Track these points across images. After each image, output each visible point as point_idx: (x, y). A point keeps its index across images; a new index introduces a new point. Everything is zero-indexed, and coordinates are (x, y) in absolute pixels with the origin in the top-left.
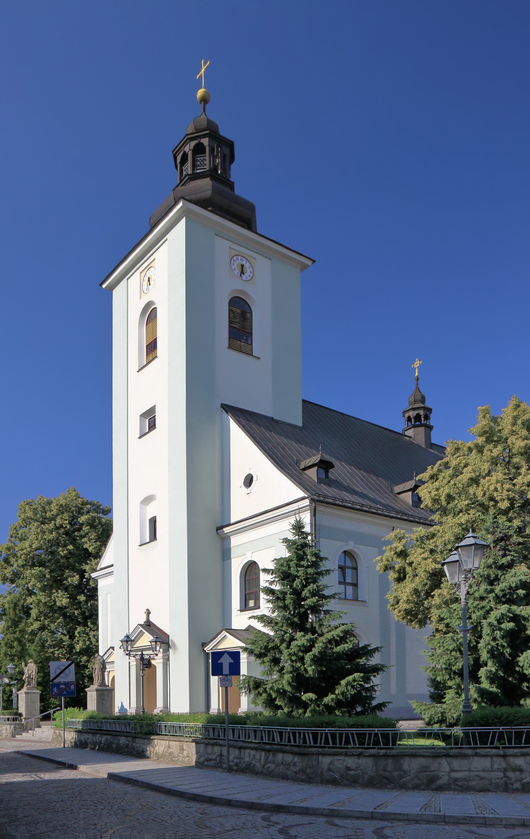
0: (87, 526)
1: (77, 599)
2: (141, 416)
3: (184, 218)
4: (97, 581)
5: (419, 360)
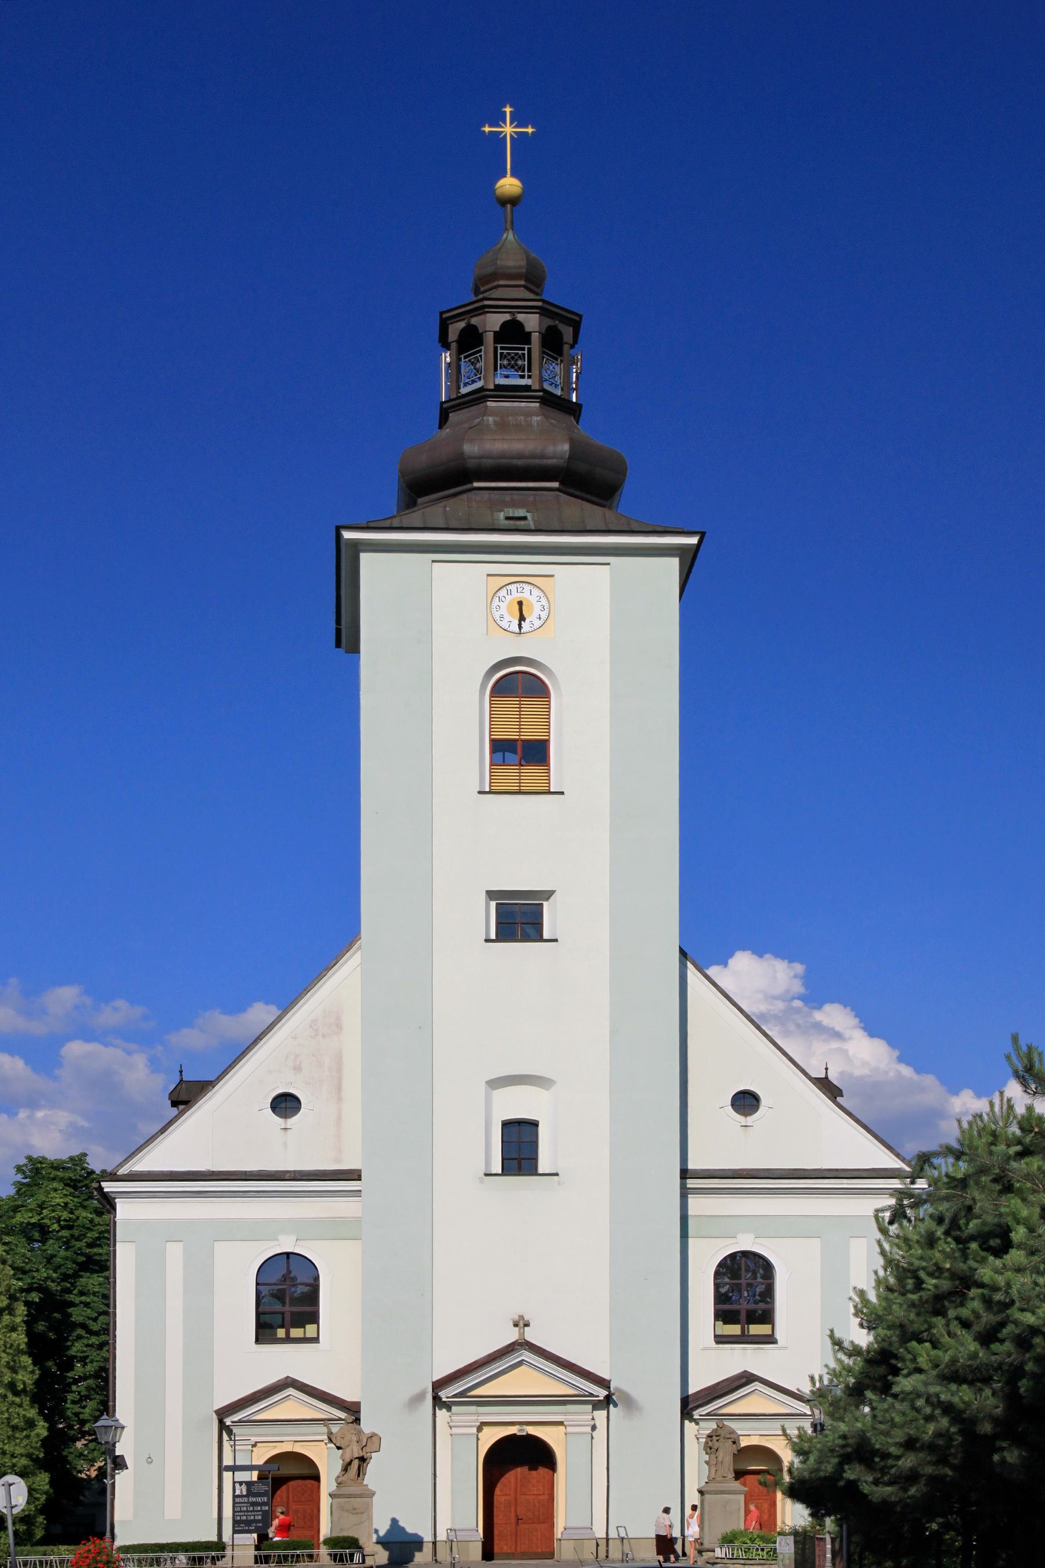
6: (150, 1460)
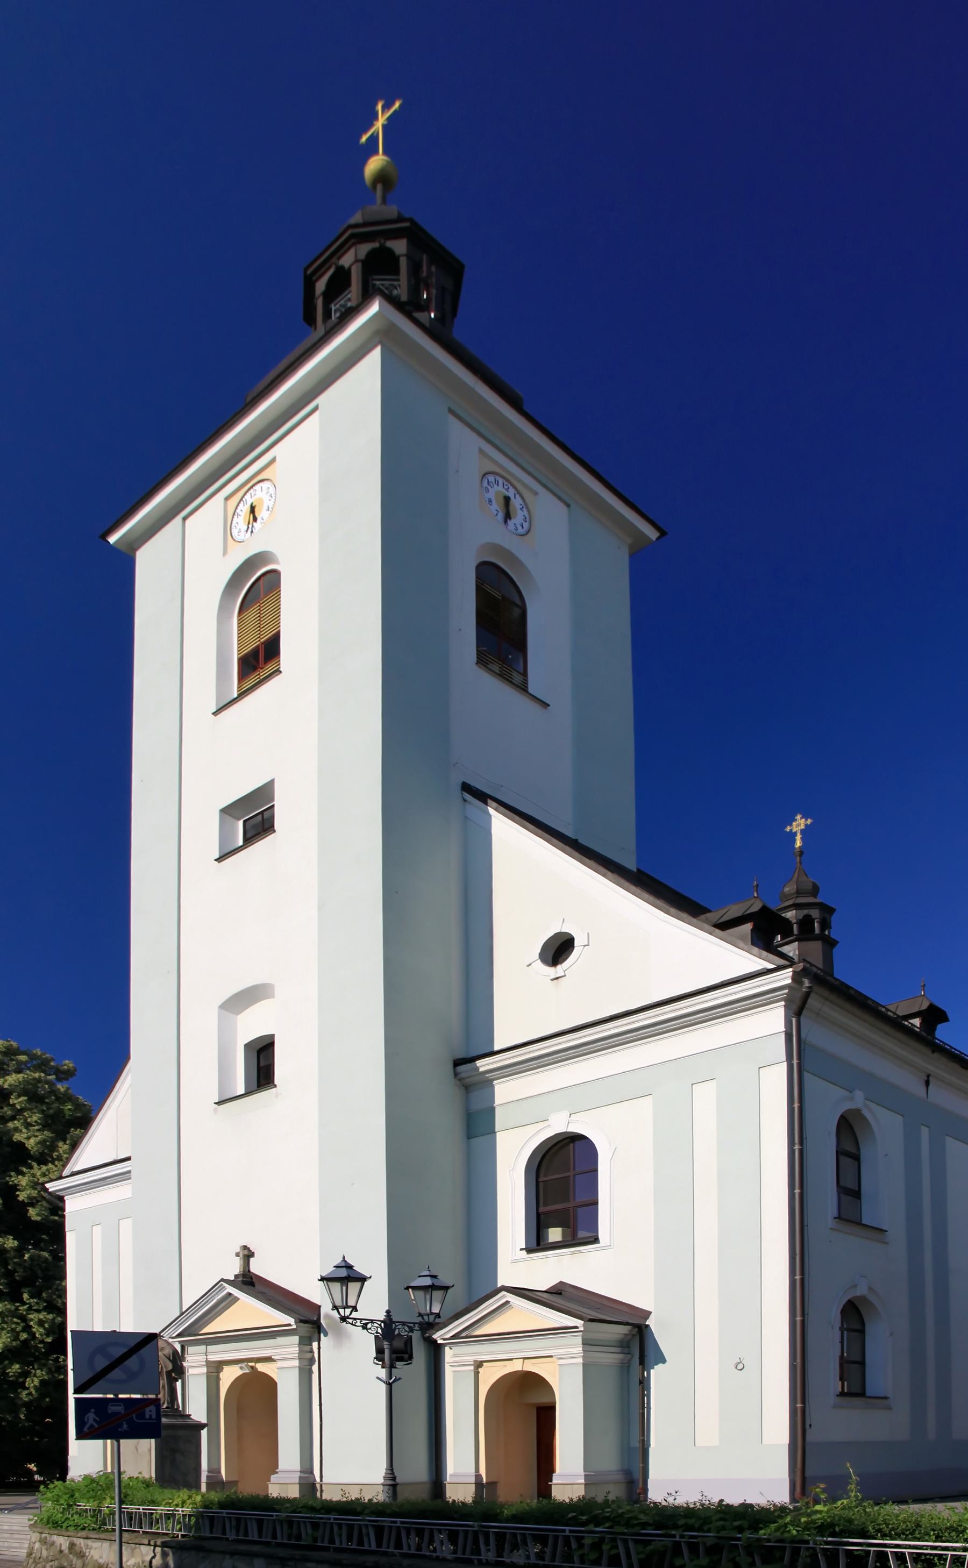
0: (19, 1096)
4: (62, 1199)
5: (805, 816)
6: (740, 1366)
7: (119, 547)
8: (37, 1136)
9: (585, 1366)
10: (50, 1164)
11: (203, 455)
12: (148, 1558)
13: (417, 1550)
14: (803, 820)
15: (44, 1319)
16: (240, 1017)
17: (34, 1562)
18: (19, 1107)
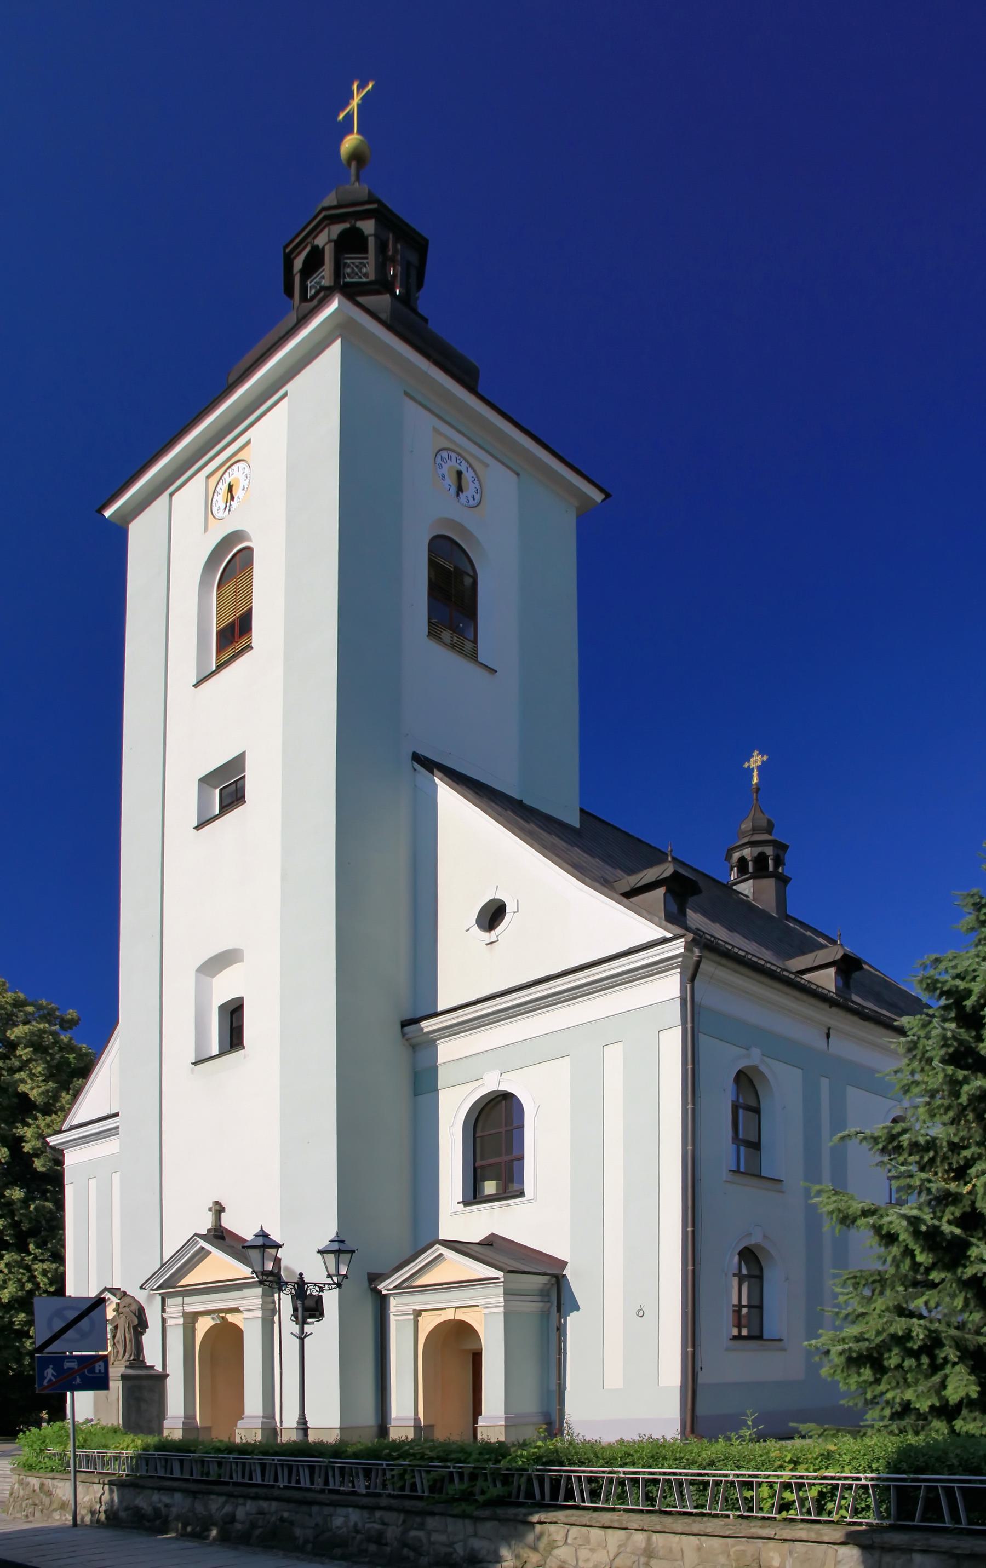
0: (25, 1047)
1: (4, 1196)
2: (200, 780)
3: (339, 341)
4: (61, 1152)
5: (762, 753)
6: (641, 1313)
7: (113, 520)
8: (40, 1087)
9: (507, 1315)
10: (53, 1115)
11: (186, 436)
12: (99, 1495)
13: (296, 1484)
14: (760, 756)
15: (48, 1269)
16: (214, 979)
17: (14, 1501)
18: (25, 1059)
